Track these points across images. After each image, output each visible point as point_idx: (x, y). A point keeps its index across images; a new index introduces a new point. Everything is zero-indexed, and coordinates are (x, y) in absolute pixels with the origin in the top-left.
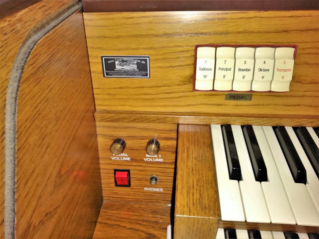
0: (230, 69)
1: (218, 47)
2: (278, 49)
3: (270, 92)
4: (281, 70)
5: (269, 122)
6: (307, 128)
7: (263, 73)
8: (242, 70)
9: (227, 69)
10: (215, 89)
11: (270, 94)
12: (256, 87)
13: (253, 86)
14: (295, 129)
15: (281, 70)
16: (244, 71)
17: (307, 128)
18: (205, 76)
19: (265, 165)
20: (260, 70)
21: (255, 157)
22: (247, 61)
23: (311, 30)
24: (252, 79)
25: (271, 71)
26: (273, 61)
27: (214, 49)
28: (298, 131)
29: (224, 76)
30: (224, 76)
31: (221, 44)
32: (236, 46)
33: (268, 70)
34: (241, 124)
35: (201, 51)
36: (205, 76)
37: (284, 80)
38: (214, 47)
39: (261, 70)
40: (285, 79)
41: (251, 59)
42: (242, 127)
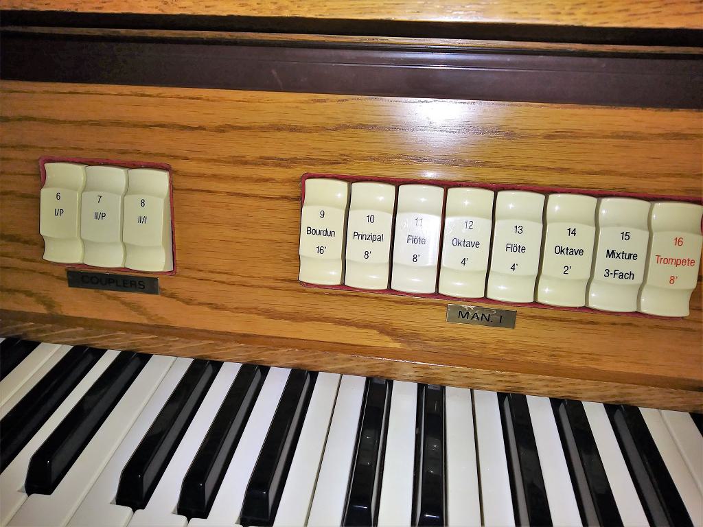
0: (381, 239)
1: (501, 190)
2: (658, 205)
3: (585, 308)
4: (668, 261)
5: (29, 329)
6: (587, 406)
7: (565, 259)
8: (316, 232)
9: (372, 238)
10: (489, 296)
11: (437, 301)
12: (551, 294)
13: (592, 295)
14: (611, 409)
15: (668, 261)
16: (320, 234)
17: (640, 409)
18: (320, 250)
19: (619, 515)
20: (557, 251)
21: (590, 489)
22: (634, 233)
23: (71, 122)
24: (588, 277)
25: (601, 253)
26: (647, 233)
27: (542, 197)
28: (618, 416)
29: (367, 254)
30: (367, 254)
31: (676, 198)
32: (600, 194)
33: (581, 252)
34: (502, 387)
35: (314, 187)
36: (320, 250)
37: (676, 286)
38: (393, 184)
39: (561, 251)
40: (679, 284)
41: (488, 218)
42: (501, 397)
